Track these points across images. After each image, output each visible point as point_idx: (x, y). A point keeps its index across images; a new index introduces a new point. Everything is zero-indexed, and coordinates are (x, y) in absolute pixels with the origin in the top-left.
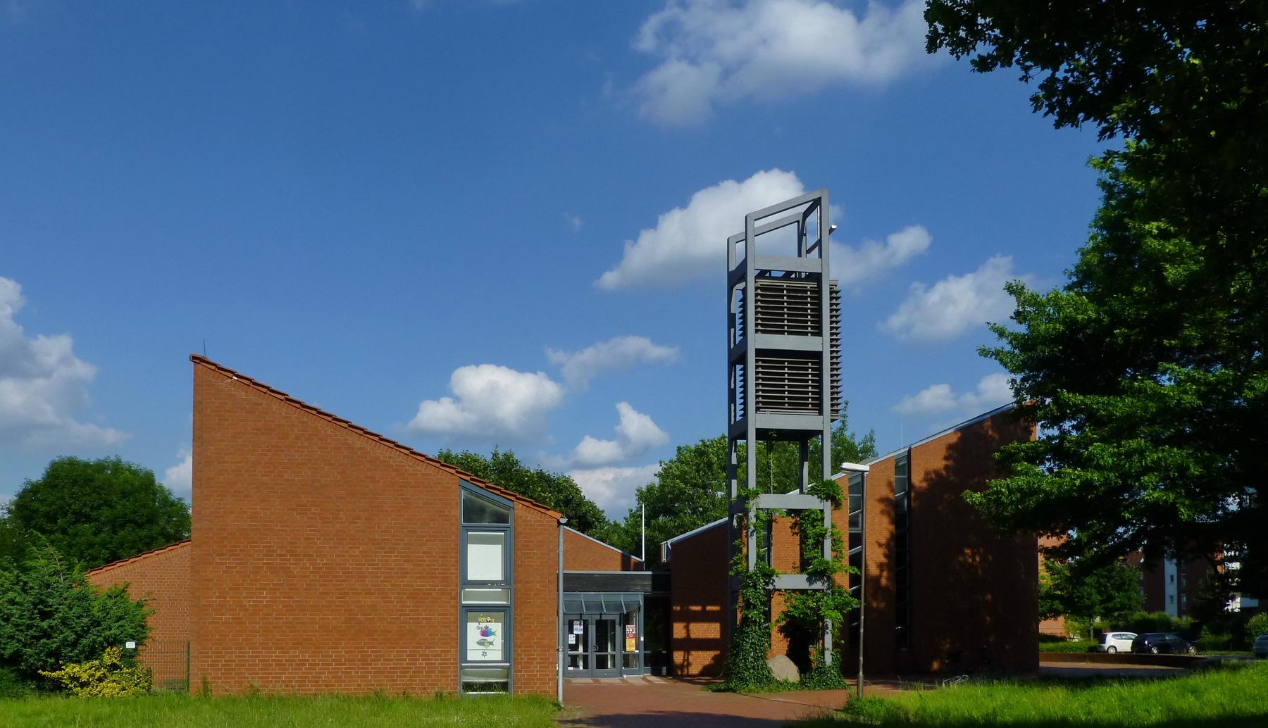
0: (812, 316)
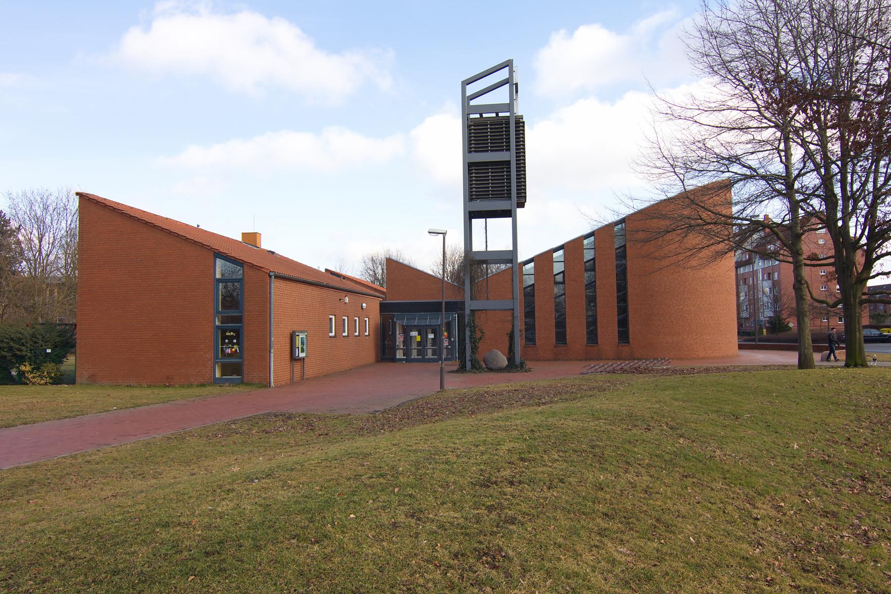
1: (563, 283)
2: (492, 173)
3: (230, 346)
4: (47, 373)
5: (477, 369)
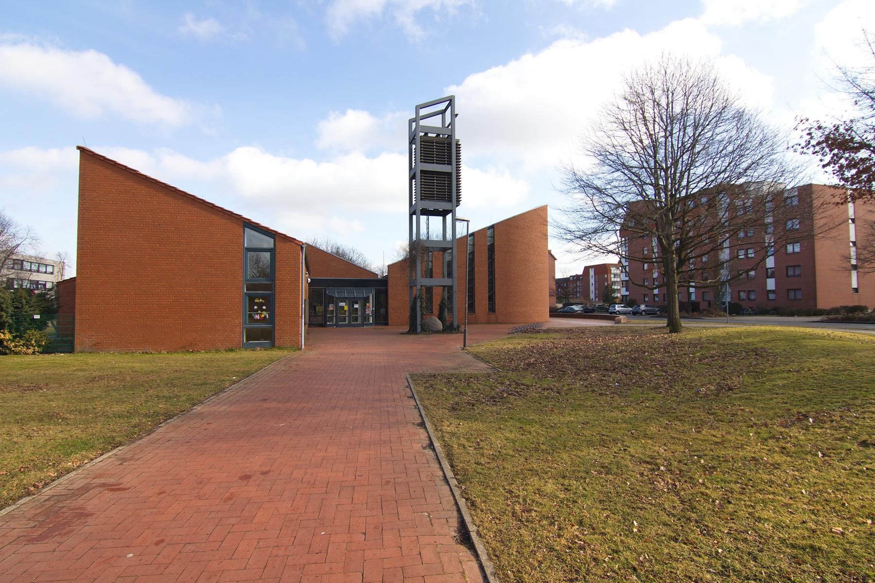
0: (448, 187)
1: (749, 299)
2: (436, 180)
3: (260, 312)
4: (35, 341)
5: (425, 331)
